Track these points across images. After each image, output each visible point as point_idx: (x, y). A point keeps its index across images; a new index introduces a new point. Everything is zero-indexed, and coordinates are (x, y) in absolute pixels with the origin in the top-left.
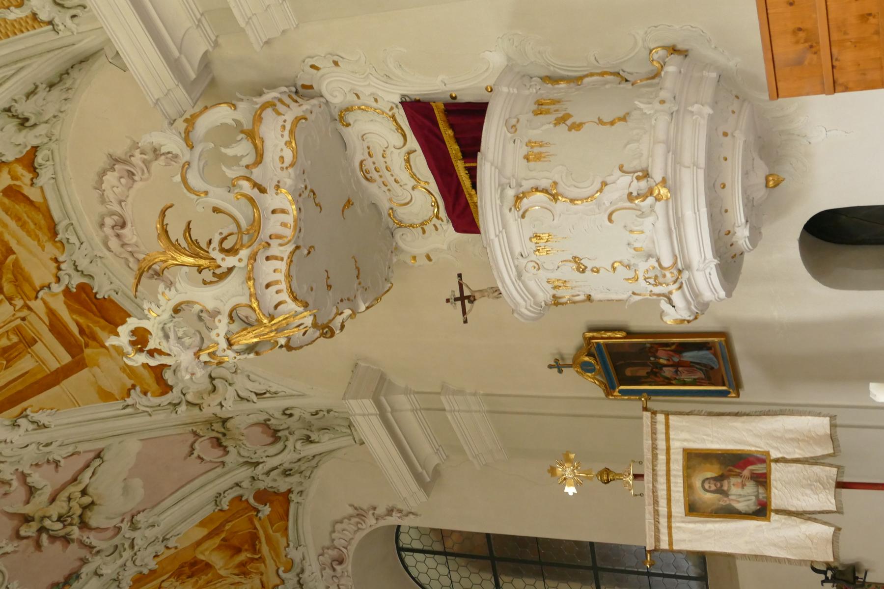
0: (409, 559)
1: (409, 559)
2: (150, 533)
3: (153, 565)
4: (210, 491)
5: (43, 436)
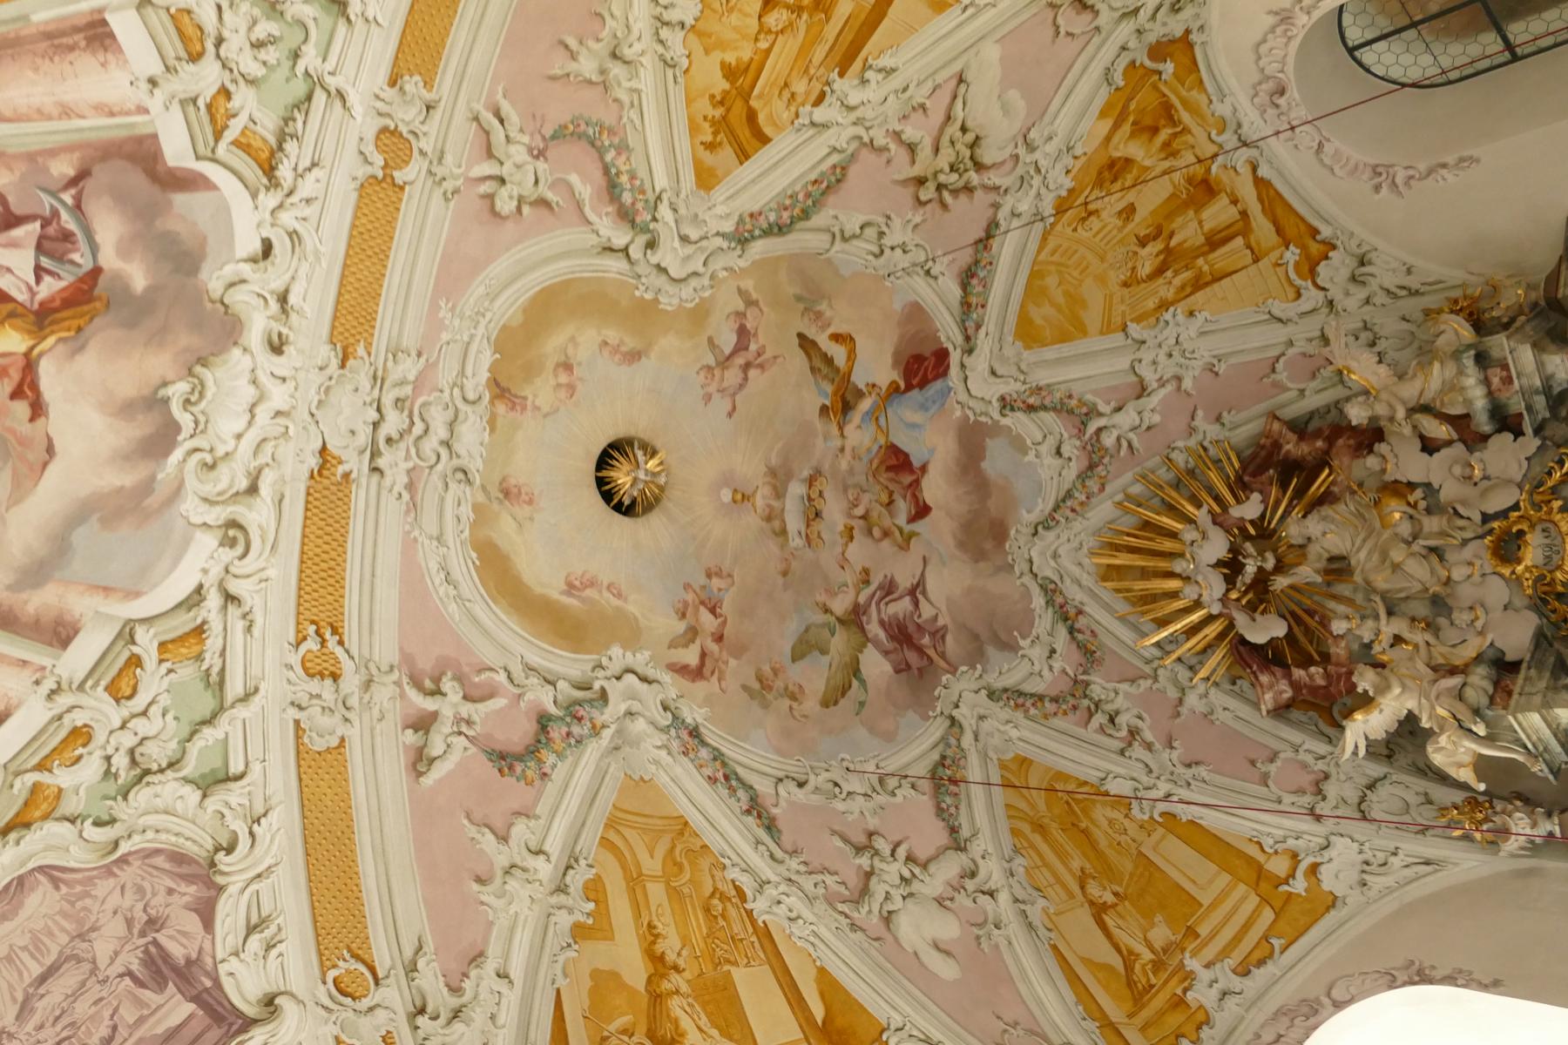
0: (1367, 56)
1: (1367, 56)
2: (1051, 148)
3: (1068, 183)
4: (1096, 71)
5: (896, 82)
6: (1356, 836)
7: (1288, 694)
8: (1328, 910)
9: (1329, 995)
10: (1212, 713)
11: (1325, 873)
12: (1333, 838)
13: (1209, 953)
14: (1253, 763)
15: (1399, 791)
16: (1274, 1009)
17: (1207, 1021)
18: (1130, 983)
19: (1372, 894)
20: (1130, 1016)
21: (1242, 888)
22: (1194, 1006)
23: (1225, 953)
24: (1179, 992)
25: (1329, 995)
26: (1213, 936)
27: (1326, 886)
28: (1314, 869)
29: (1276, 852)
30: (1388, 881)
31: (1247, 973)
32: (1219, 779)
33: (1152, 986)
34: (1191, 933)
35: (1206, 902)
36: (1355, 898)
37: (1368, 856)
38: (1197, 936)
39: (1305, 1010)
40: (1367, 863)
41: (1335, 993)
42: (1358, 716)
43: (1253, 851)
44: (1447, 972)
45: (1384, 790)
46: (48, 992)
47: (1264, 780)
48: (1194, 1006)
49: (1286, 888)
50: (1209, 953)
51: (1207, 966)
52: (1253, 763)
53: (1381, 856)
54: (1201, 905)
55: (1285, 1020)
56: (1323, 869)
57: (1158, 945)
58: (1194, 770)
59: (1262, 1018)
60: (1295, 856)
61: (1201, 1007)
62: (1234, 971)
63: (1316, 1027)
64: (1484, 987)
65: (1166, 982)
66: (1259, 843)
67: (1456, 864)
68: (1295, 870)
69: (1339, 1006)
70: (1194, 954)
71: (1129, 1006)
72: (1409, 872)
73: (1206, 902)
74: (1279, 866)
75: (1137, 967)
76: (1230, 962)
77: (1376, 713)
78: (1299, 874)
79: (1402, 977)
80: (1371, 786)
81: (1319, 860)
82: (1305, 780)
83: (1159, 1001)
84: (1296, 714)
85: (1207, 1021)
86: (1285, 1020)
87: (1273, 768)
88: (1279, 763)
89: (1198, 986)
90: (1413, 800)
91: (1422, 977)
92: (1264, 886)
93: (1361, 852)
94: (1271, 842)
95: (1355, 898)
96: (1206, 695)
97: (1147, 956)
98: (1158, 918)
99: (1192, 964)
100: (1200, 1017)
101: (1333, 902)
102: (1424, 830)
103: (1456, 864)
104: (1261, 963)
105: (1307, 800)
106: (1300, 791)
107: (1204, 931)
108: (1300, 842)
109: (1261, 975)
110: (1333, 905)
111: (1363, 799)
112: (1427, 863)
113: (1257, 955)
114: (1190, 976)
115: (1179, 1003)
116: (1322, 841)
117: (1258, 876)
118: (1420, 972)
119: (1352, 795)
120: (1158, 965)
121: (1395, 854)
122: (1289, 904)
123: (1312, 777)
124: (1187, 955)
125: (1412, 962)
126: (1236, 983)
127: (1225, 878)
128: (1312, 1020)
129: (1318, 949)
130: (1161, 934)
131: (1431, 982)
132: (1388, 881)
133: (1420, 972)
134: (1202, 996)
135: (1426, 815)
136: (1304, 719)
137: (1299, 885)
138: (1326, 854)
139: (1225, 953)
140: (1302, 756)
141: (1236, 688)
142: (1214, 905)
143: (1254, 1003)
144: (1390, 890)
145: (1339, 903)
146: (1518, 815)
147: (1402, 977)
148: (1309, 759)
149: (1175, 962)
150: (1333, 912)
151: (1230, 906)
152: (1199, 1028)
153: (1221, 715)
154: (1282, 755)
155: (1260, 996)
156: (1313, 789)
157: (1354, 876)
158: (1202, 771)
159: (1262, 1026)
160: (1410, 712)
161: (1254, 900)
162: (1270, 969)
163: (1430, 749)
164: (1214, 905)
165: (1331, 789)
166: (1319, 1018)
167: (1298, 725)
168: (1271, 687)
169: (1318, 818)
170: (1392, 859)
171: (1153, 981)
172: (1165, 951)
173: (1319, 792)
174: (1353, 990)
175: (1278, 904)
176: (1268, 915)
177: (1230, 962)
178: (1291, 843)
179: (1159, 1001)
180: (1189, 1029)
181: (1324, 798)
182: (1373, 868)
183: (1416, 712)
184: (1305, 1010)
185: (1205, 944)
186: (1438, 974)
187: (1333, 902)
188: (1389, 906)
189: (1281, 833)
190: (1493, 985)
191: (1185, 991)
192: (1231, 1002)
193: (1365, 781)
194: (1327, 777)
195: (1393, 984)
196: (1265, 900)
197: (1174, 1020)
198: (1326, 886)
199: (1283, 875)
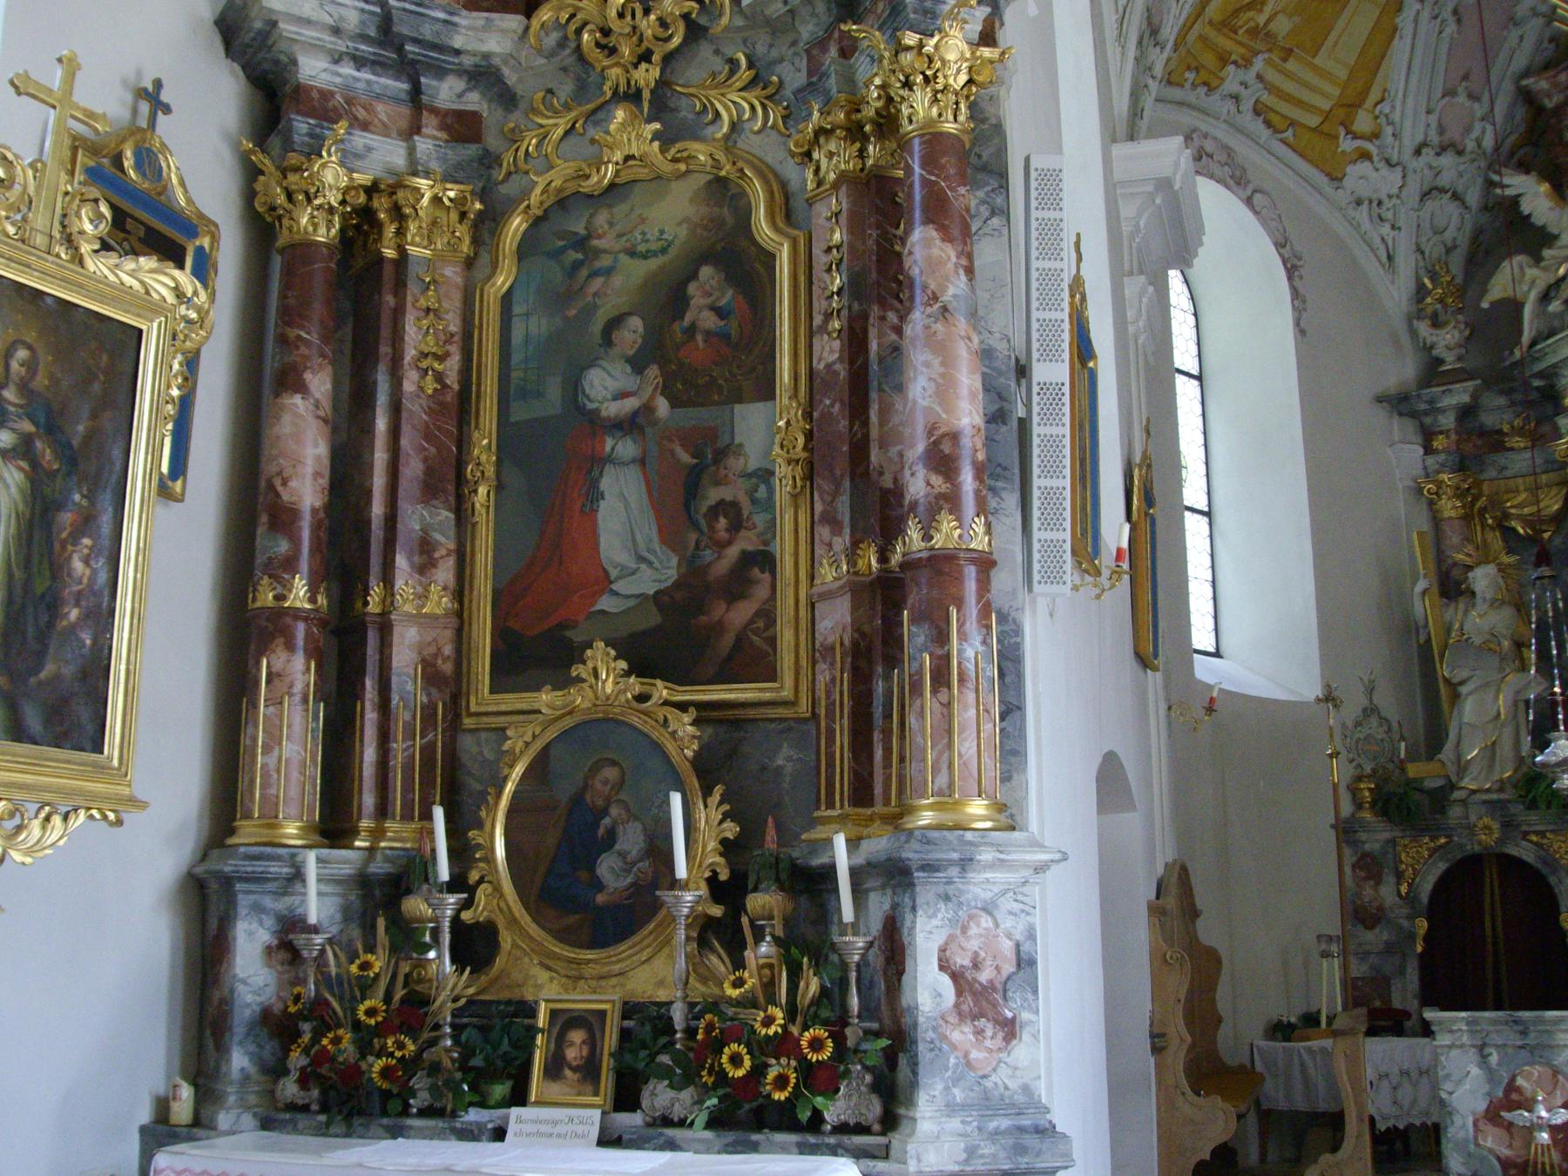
6: (1405, 191)
7: (1549, 104)
8: (1327, 175)
9: (1255, 191)
10: (1516, 25)
11: (1363, 167)
12: (1399, 169)
13: (1271, 75)
14: (1466, 77)
15: (1455, 220)
16: (1231, 144)
17: (1211, 89)
18: (1236, 12)
19: (1351, 212)
20: (1210, 23)
21: (1336, 92)
22: (1223, 74)
23: (1271, 88)
24: (1233, 57)
25: (1255, 191)
26: (1288, 75)
27: (1350, 169)
28: (1365, 156)
29: (1377, 118)
30: (1366, 225)
31: (1257, 112)
32: (1444, 48)
33: (1236, 32)
34: (1288, 53)
35: (1317, 61)
36: (1342, 197)
37: (1387, 204)
38: (1285, 60)
39: (1238, 173)
40: (1380, 203)
41: (1257, 197)
42: (1545, 187)
43: (1374, 96)
44: (1301, 290)
45: (1453, 209)
46: (499, 1134)
47: (1450, 93)
48: (1223, 74)
49: (1343, 133)
50: (1271, 75)
51: (1259, 77)
52: (1466, 77)
53: (1389, 215)
54: (1314, 56)
55: (1224, 158)
56: (1367, 164)
57: (1272, 26)
58: (1451, 20)
59: (1220, 135)
60: (1375, 136)
61: (1223, 79)
62: (1257, 101)
63: (1227, 187)
64: (1297, 323)
65: (1240, 43)
66: (1382, 100)
67: (1393, 282)
68: (1362, 138)
69: (1249, 201)
70: (1268, 62)
71: (1217, 18)
72: (1377, 241)
73: (1317, 61)
74: (1363, 122)
75: (1251, 14)
76: (1266, 97)
77: (1551, 204)
78: (1358, 143)
79: (1286, 252)
80: (1456, 197)
81: (1376, 159)
82: (1454, 133)
83: (1225, 43)
84: (1521, 112)
85: (1211, 89)
86: (1224, 158)
87: (1462, 99)
88: (1468, 104)
89: (1241, 72)
90: (1448, 236)
91: (1291, 271)
92: (1342, 112)
93: (1390, 197)
94: (1387, 110)
95: (1342, 197)
96: (1536, 14)
97: (1262, 19)
98: (1297, 19)
99: (1259, 64)
100: (1214, 83)
101: (1336, 179)
102: (1420, 251)
103: (1393, 282)
104: (1268, 124)
105: (1434, 137)
106: (1442, 130)
107: (1291, 65)
108: (1390, 139)
109: (1258, 127)
110: (1333, 179)
111: (1443, 191)
112: (1390, 258)
113: (1275, 119)
114: (1248, 63)
115: (1224, 60)
116: (1395, 159)
117: (1351, 105)
118: (1294, 267)
119: (1445, 180)
120: (1254, 32)
121: (1393, 227)
122: (1327, 138)
123: (1457, 138)
124: (1266, 56)
125: (1300, 259)
126: (1247, 105)
127: (1343, 74)
128: (1231, 182)
129: (1290, 172)
130: (1282, 26)
131: (1290, 278)
132: (1366, 225)
133: (1294, 267)
134: (1232, 78)
135: (1434, 249)
136: (1518, 117)
137: (1347, 145)
138: (1382, 165)
139: (1271, 88)
140: (1478, 127)
141: (1546, 44)
142: (1315, 68)
143: (1232, 125)
144: (1357, 227)
145: (1336, 184)
146: (1457, 334)
147: (1286, 252)
148: (1475, 134)
149: (1258, 46)
150: (1326, 179)
151: (1318, 83)
152: (1205, 84)
153: (1514, 34)
154: (1476, 106)
155: (1239, 130)
156: (1446, 142)
157: (1365, 192)
158: (1451, 28)
159: (1215, 138)
160: (1556, 237)
161: (1326, 105)
162: (1265, 133)
163: (1519, 259)
164: (1315, 69)
165: (1447, 160)
166: (1235, 188)
167: (1510, 116)
168: (1556, 85)
169: (1418, 152)
170: (1387, 226)
171: (1241, 32)
172: (1268, 34)
173: (1442, 150)
174: (1264, 211)
175: (1325, 128)
176: (1313, 121)
177: (1266, 97)
178: (1389, 130)
179: (1225, 43)
180: (1204, 75)
181: (1438, 154)
182: (1376, 210)
183: (1559, 243)
184: (1238, 173)
185: (1275, 67)
186: (1297, 282)
187: (1336, 179)
188: (1341, 229)
189: (1396, 117)
190: (1301, 331)
191: (1235, 63)
192: (1230, 105)
193: (1460, 189)
194: (1460, 153)
195: (1279, 246)
196: (1327, 116)
197: (1209, 59)
198: (1350, 169)
199: (1355, 128)
